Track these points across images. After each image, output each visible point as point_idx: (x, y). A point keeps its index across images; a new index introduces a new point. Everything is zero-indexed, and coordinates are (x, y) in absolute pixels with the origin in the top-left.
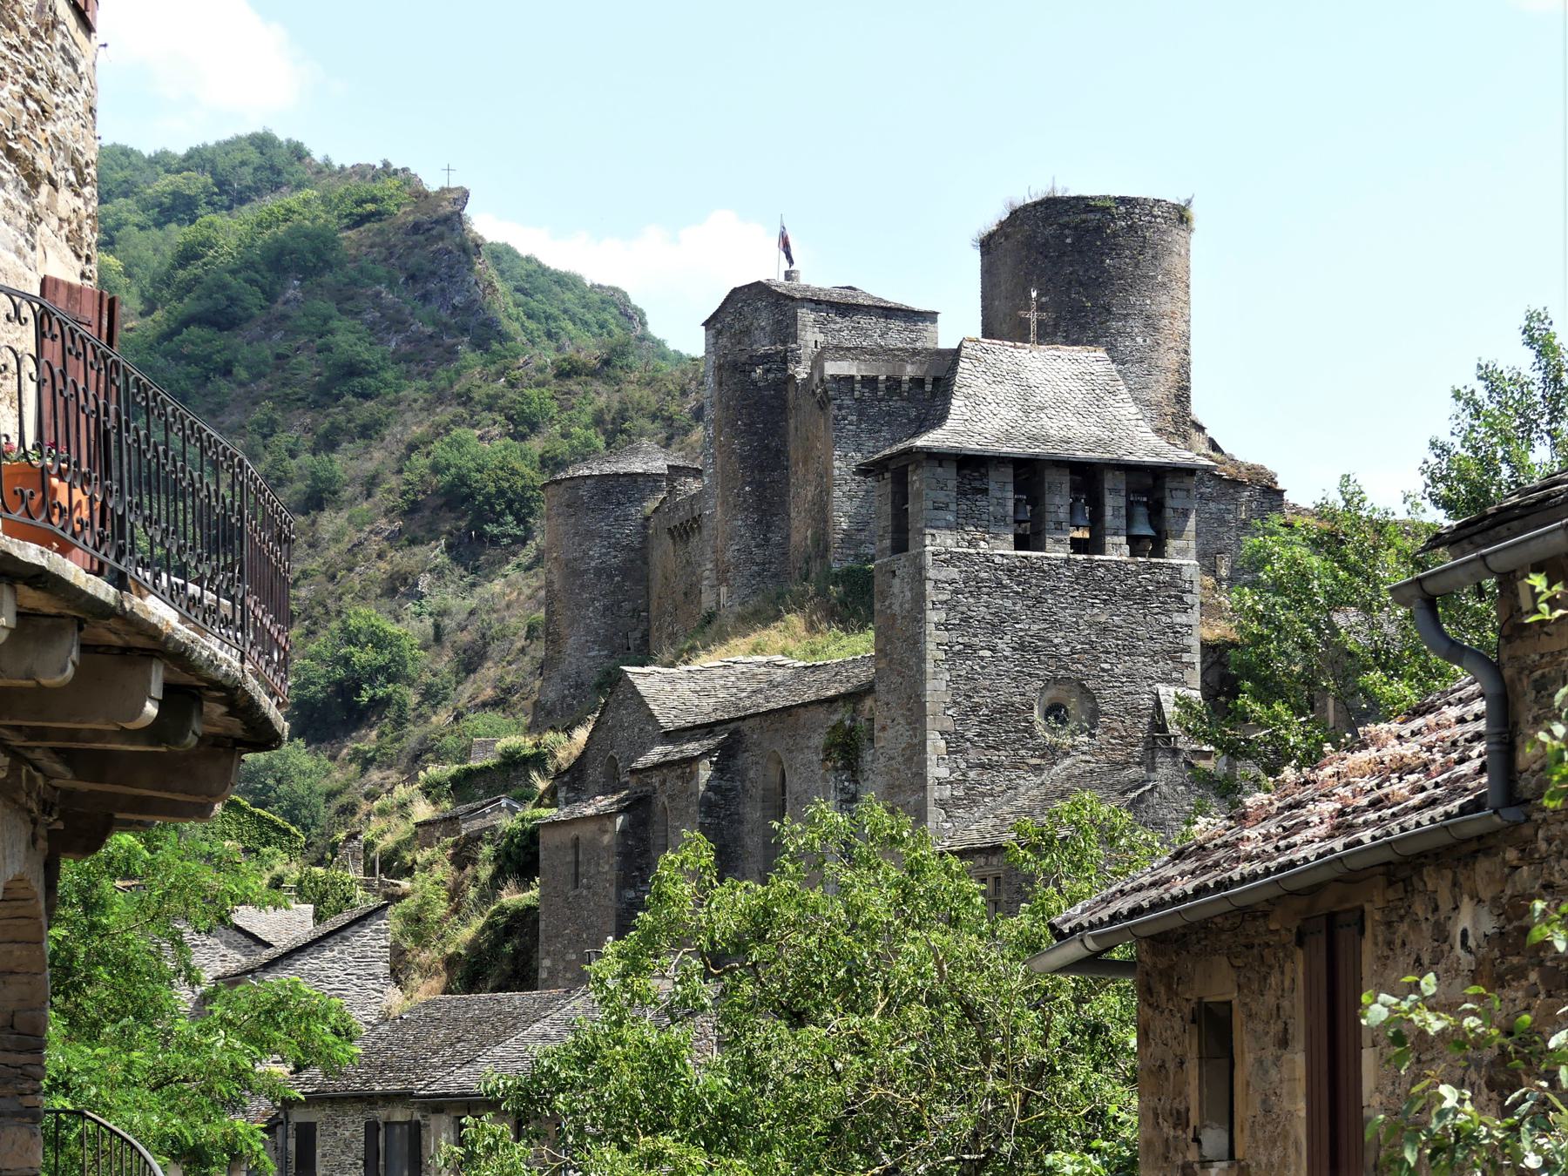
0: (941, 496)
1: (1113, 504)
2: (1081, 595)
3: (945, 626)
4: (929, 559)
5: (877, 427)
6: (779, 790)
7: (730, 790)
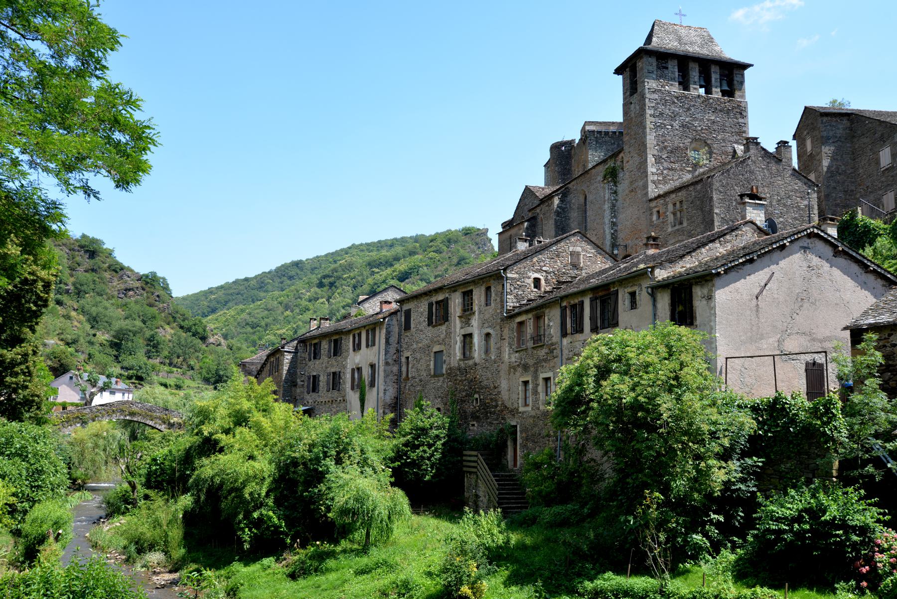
0: (651, 68)
1: (715, 77)
4: (647, 91)
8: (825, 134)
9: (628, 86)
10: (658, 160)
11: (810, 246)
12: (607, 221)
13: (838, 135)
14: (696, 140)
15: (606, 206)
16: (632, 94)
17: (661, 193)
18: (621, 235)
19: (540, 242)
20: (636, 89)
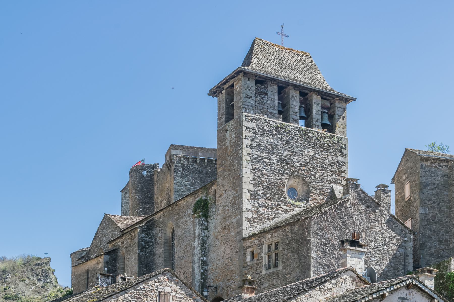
0: (249, 93)
2: (303, 143)
3: (250, 147)
5: (189, 173)
6: (171, 239)
7: (151, 242)
8: (424, 180)
9: (224, 111)
10: (254, 196)
11: (408, 297)
12: (196, 259)
13: (437, 182)
14: (294, 176)
15: (196, 243)
16: (227, 121)
17: (256, 231)
18: (211, 276)
19: (125, 279)
20: (233, 115)
